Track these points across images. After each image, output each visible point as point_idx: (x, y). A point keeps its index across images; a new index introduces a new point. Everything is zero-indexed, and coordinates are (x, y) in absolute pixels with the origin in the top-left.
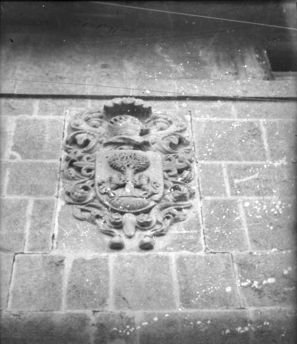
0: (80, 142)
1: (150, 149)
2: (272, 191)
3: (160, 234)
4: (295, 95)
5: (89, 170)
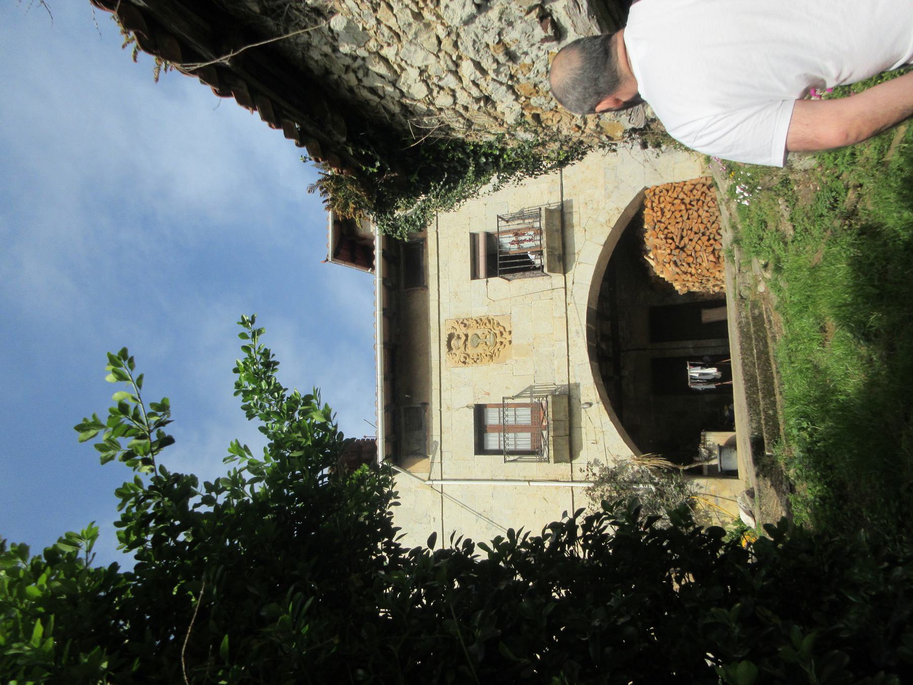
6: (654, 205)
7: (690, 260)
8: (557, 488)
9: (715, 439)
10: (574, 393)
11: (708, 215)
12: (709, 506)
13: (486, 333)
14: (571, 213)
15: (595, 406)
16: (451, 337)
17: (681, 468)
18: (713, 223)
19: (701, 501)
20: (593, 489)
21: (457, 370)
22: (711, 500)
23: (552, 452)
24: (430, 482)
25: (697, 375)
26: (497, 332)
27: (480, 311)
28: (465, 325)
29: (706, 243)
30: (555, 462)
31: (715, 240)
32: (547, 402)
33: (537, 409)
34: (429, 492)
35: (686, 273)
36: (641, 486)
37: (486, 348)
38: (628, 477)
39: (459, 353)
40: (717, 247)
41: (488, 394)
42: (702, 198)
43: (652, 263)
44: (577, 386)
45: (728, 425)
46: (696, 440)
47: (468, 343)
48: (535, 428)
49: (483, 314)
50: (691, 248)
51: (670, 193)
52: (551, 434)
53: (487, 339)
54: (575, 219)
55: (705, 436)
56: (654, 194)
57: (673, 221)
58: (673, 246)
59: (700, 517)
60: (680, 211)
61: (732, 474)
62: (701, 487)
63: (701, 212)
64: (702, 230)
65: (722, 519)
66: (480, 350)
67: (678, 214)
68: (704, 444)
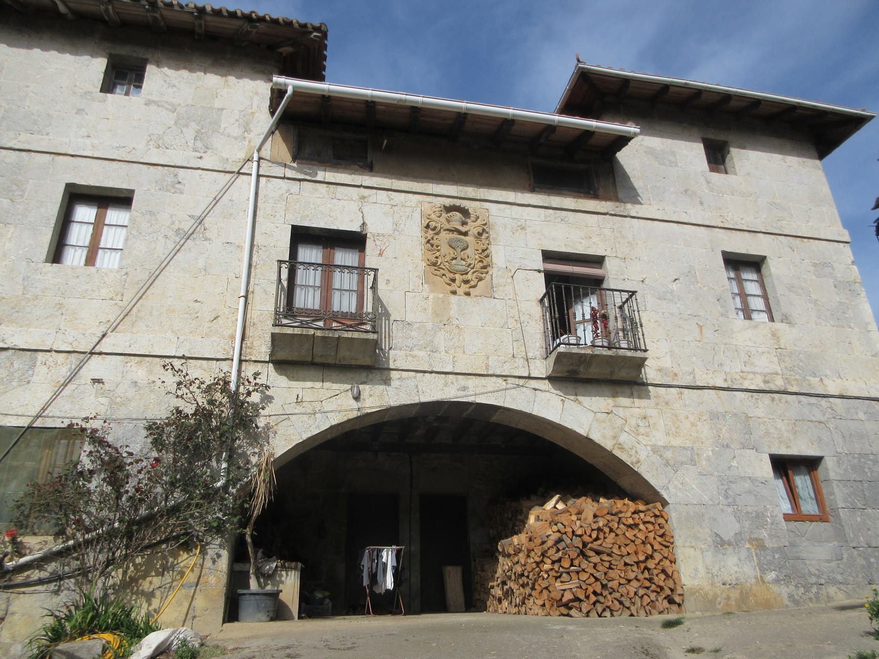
0: (432, 227)
1: (620, 195)
2: (219, 489)
3: (474, 287)
4: (93, 221)
5: (437, 246)
6: (642, 515)
7: (566, 563)
8: (233, 337)
9: (289, 585)
10: (377, 375)
11: (632, 594)
12: (182, 574)
13: (469, 261)
14: (631, 396)
15: (354, 404)
16: (465, 212)
17: (248, 531)
18: (621, 603)
19: (192, 561)
20: (225, 389)
21: (417, 215)
22: (191, 577)
23: (289, 331)
24: (256, 158)
25: (384, 560)
26: (469, 276)
27: (499, 255)
28: (480, 234)
29: (590, 589)
30: (274, 336)
31: (594, 604)
32: (367, 332)
33: (356, 319)
34: (242, 155)
35: (543, 555)
36: (224, 465)
37: (448, 258)
38: (240, 447)
39: (441, 222)
40: (585, 607)
41: (380, 254)
42: (653, 587)
43: (549, 505)
44: (387, 382)
45: (310, 608)
46: (289, 555)
47: (455, 235)
48: (325, 313)
49: (494, 260)
50: (583, 566)
51: (659, 539)
52: (319, 333)
53: (458, 262)
54: (624, 401)
55: (295, 569)
56: (656, 516)
57: (621, 540)
58: (586, 538)
59: (164, 558)
60: (636, 553)
61: (232, 614)
62: (214, 562)
63: (635, 584)
64: (610, 584)
65: (158, 593)
66: (445, 249)
67: (631, 549)
68: (283, 567)
